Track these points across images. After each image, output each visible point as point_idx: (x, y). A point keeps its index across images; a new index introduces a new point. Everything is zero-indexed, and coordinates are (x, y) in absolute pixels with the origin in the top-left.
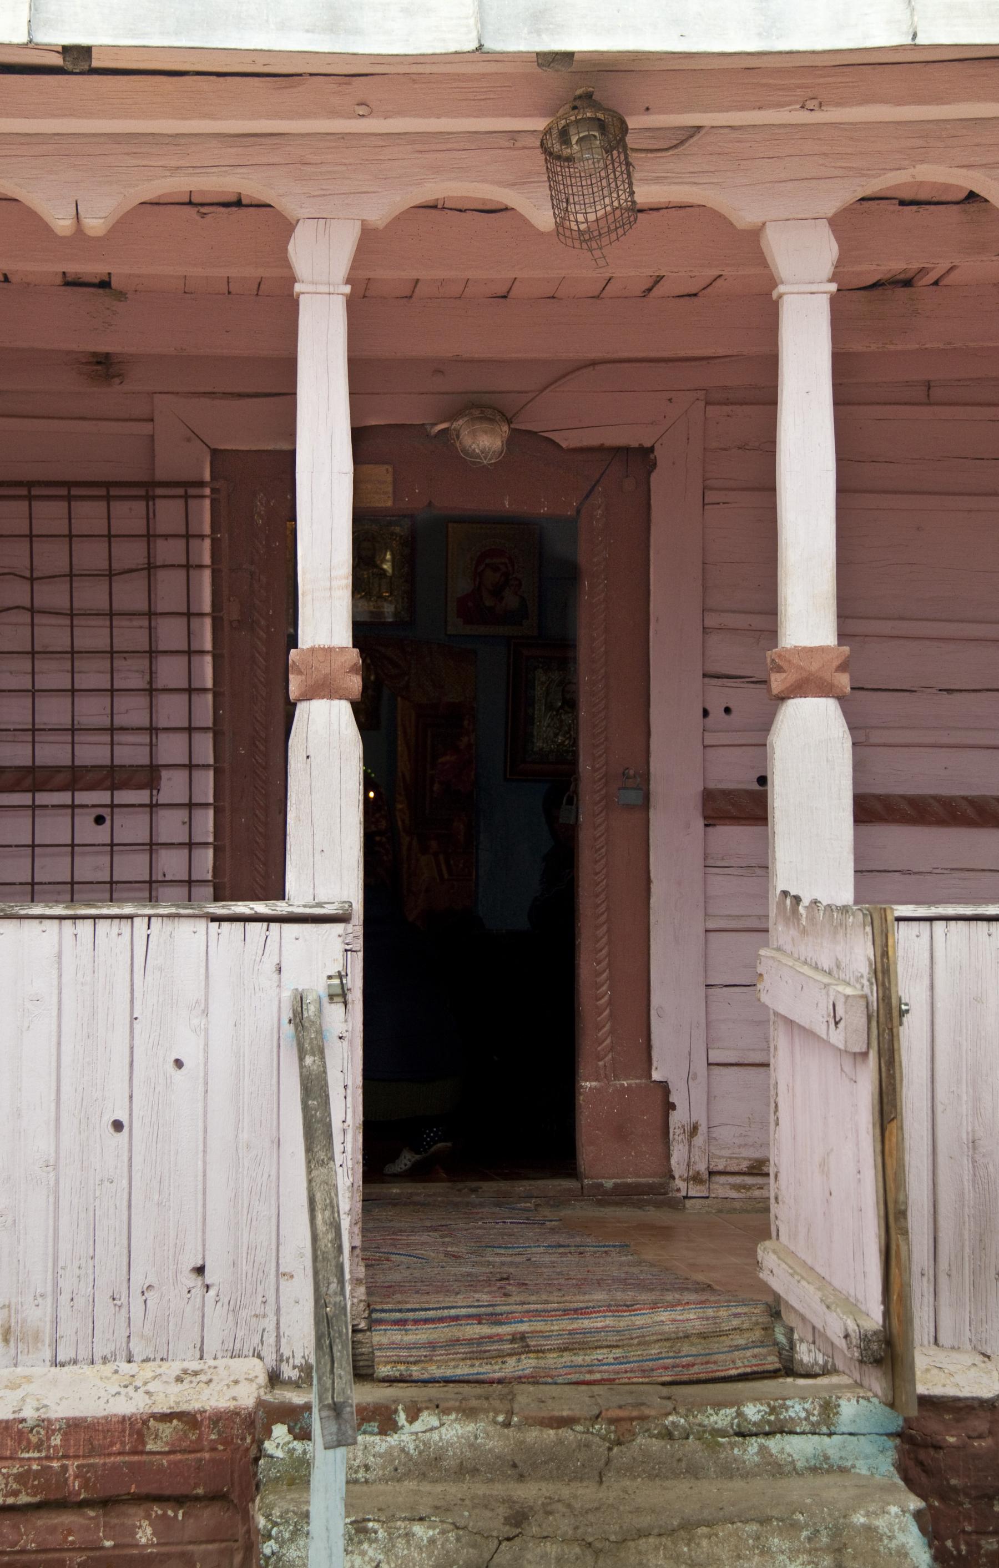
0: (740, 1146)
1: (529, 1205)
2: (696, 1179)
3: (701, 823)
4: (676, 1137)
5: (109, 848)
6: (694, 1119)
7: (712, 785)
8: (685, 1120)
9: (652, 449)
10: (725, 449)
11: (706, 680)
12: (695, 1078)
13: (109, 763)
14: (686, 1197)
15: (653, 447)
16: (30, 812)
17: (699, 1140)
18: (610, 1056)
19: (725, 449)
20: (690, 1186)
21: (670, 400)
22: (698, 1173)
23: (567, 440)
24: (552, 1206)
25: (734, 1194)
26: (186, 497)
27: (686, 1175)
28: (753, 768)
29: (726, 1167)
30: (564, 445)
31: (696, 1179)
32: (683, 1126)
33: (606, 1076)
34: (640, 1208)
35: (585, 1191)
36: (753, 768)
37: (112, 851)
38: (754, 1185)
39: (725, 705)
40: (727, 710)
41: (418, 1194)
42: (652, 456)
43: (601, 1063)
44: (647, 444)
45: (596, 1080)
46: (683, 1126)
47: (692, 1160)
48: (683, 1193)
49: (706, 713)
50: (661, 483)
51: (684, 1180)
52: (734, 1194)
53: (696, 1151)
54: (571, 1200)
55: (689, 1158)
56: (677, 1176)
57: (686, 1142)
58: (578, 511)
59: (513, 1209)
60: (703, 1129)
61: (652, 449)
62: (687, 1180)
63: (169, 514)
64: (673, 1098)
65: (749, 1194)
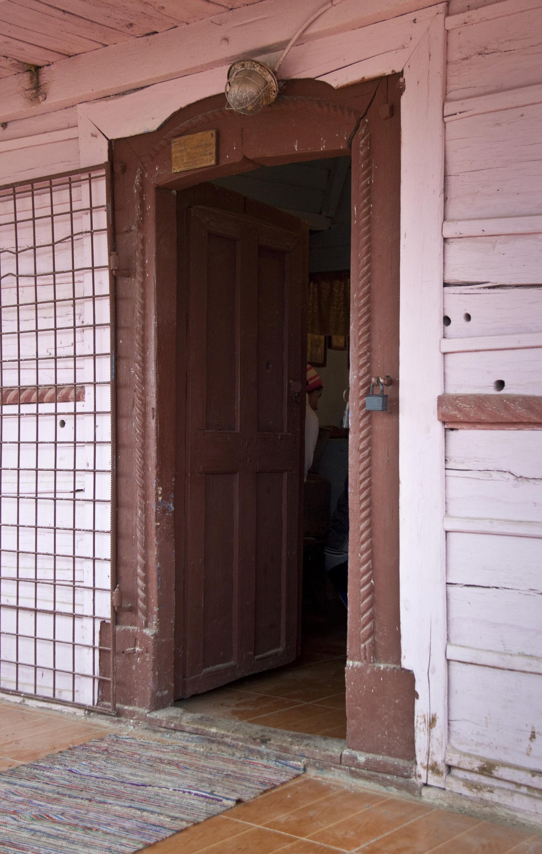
0: (477, 744)
1: (299, 763)
2: (433, 768)
3: (438, 428)
4: (418, 724)
5: (73, 445)
6: (433, 711)
7: (452, 391)
8: (426, 711)
9: (401, 74)
10: (467, 58)
11: (447, 289)
12: (434, 672)
13: (35, 384)
14: (426, 785)
15: (403, 71)
16: (35, 418)
17: (439, 730)
18: (370, 640)
19: (467, 58)
20: (429, 775)
21: (415, 21)
22: (436, 763)
23: (337, 81)
24: (318, 768)
25: (466, 792)
26: (90, 179)
27: (426, 764)
28: (489, 372)
29: (459, 763)
30: (334, 84)
31: (433, 768)
32: (424, 716)
33: (365, 658)
34: (385, 786)
35: (343, 761)
36: (489, 372)
37: (75, 446)
38: (485, 786)
39: (464, 312)
40: (468, 317)
41: (227, 737)
42: (401, 80)
43: (362, 646)
44: (398, 70)
45: (360, 660)
46: (424, 716)
47: (431, 750)
48: (424, 780)
49: (447, 321)
50: (407, 104)
51: (424, 768)
52: (466, 792)
53: (434, 742)
54: (331, 766)
55: (429, 748)
56: (419, 763)
57: (426, 731)
58: (350, 146)
59: (286, 765)
60: (441, 721)
61: (401, 74)
62: (427, 768)
63: (81, 192)
64: (418, 688)
65: (480, 795)
